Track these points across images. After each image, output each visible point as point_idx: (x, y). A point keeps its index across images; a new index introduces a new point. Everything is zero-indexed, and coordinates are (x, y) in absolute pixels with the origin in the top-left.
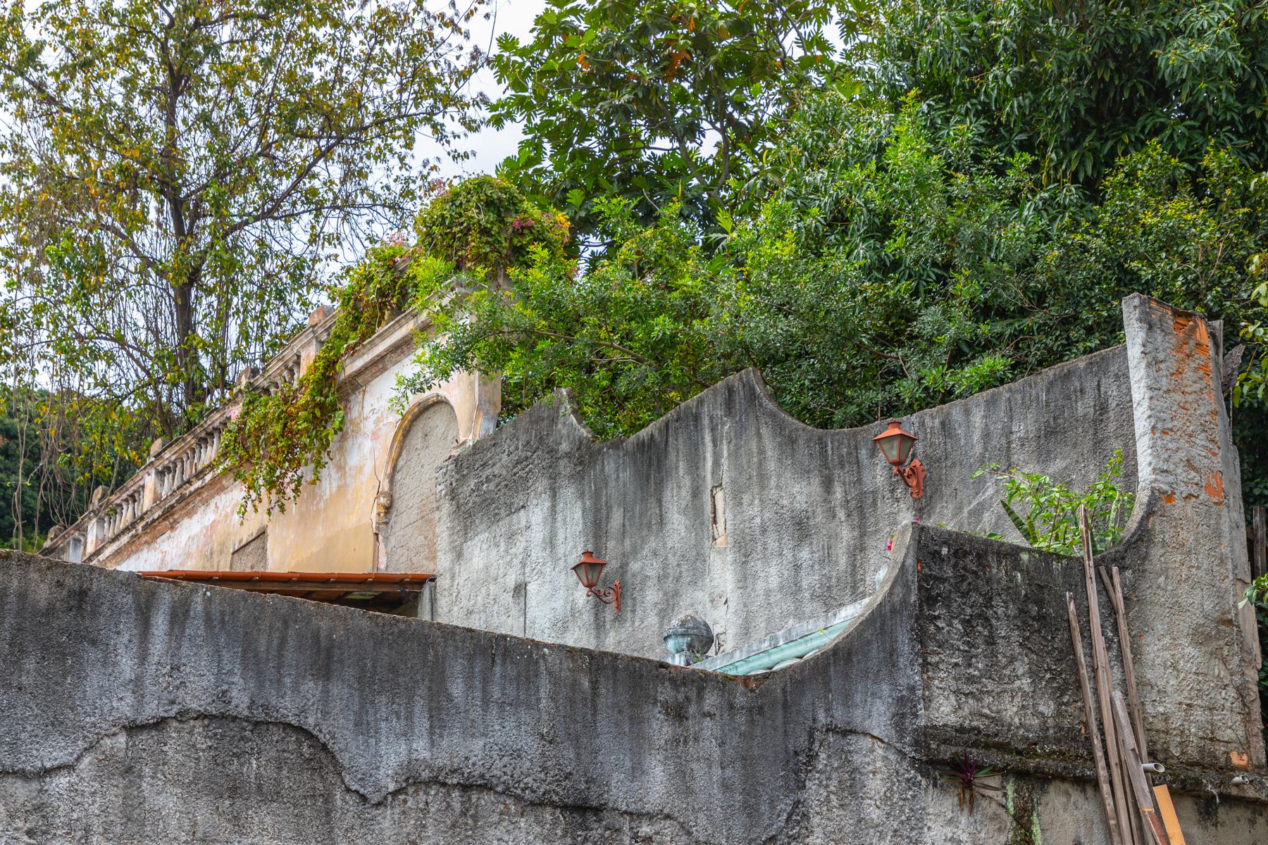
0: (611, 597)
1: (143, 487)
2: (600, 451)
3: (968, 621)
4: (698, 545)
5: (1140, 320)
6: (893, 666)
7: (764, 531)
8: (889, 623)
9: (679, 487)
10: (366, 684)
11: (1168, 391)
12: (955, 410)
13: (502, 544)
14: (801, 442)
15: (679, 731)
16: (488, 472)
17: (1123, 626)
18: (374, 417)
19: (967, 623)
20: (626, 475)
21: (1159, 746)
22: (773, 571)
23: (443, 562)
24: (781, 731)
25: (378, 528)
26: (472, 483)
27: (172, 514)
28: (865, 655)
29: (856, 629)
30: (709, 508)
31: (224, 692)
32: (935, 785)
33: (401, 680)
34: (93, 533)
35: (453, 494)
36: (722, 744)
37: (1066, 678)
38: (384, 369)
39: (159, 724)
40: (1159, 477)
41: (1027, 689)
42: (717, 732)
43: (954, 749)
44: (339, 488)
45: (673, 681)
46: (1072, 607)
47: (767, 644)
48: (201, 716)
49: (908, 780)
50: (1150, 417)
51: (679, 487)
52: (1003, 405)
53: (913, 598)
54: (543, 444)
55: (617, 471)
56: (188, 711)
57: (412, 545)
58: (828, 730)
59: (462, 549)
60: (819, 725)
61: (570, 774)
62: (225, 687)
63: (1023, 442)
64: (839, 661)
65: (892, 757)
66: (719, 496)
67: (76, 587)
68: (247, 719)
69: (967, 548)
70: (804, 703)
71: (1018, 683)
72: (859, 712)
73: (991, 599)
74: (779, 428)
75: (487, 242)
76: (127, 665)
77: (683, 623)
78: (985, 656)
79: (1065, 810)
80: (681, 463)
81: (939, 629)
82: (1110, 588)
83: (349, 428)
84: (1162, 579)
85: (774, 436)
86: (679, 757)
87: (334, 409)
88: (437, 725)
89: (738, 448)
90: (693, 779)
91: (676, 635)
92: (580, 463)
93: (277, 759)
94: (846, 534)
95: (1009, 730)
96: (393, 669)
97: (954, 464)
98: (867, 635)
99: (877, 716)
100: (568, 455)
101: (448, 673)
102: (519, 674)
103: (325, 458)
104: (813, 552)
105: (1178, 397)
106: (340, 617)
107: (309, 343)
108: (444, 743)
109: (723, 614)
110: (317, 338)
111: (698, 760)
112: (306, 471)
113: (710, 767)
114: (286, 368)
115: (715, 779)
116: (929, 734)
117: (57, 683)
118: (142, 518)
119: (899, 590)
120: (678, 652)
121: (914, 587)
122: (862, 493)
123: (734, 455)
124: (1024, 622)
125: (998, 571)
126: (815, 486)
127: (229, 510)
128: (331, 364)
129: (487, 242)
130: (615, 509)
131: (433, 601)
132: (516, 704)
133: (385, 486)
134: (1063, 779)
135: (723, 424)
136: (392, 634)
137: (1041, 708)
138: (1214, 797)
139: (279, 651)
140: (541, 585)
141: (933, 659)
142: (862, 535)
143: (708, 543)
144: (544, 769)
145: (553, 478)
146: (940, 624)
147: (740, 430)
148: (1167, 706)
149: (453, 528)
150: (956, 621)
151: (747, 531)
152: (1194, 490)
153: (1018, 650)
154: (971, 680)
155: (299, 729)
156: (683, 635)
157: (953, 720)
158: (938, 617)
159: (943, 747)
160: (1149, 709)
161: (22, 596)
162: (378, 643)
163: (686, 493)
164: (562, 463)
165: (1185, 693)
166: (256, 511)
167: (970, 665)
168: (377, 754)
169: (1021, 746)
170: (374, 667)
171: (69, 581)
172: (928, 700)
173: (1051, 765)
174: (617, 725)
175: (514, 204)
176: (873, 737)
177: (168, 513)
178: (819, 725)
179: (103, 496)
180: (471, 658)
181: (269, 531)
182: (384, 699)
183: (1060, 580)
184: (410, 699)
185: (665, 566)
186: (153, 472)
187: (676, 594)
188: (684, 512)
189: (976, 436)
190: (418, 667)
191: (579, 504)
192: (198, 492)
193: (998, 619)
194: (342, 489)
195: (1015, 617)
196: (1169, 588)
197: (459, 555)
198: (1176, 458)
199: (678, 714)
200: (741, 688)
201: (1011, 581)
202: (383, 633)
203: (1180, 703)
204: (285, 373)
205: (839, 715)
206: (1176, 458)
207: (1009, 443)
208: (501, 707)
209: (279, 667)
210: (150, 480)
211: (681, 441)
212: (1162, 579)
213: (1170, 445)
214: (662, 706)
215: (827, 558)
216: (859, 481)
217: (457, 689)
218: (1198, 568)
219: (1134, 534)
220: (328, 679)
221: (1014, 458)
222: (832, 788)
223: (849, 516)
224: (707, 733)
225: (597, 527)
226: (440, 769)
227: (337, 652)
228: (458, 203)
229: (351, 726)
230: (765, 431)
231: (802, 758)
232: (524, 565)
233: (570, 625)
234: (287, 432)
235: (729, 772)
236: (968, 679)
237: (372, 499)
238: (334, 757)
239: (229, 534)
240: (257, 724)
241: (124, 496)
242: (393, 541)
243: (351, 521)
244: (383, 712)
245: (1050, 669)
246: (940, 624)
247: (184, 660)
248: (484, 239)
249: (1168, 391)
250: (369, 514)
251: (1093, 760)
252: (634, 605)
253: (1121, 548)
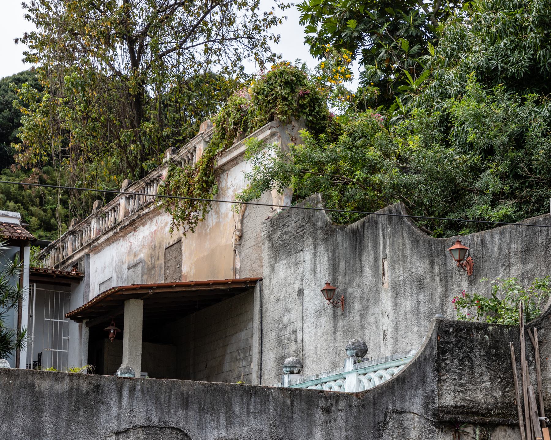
0: (340, 304)
1: (119, 204)
2: (335, 229)
4: (376, 286)
6: (424, 382)
7: (404, 283)
8: (423, 364)
9: (369, 255)
10: (201, 409)
12: (487, 234)
13: (293, 267)
14: (421, 242)
15: (328, 418)
16: (286, 229)
17: (537, 356)
18: (232, 188)
19: (460, 361)
20: (346, 244)
22: (408, 303)
23: (265, 272)
25: (236, 247)
26: (279, 233)
27: (134, 224)
28: (411, 379)
29: (407, 368)
30: (381, 268)
31: (149, 417)
32: (442, 431)
33: (215, 407)
34: (94, 225)
35: (270, 238)
36: (346, 422)
37: (508, 381)
38: (237, 164)
39: (127, 431)
41: (488, 387)
42: (344, 417)
43: (450, 416)
44: (217, 223)
45: (325, 398)
46: (512, 349)
47: (384, 360)
48: (141, 427)
49: (430, 430)
51: (369, 255)
52: (507, 235)
53: (435, 352)
55: (342, 241)
56: (136, 426)
57: (252, 258)
58: (393, 412)
59: (274, 267)
60: (389, 410)
62: (149, 416)
64: (400, 382)
65: (422, 421)
66: (386, 263)
67: (96, 384)
68: (158, 427)
70: (383, 402)
72: (407, 403)
73: (473, 349)
74: (412, 234)
75: (286, 105)
76: (114, 411)
77: (353, 344)
79: (504, 438)
80: (370, 244)
81: (447, 364)
82: (532, 338)
87: (213, 182)
90: (333, 436)
91: (350, 349)
92: (327, 234)
94: (440, 289)
95: (479, 405)
96: (212, 403)
97: (486, 261)
98: (413, 370)
99: (416, 404)
100: (321, 228)
101: (233, 403)
102: (261, 401)
103: (208, 208)
104: (425, 296)
107: (200, 141)
108: (232, 430)
109: (386, 321)
110: (204, 140)
111: (336, 429)
113: (341, 431)
114: (189, 152)
115: (343, 436)
116: (442, 409)
117: (91, 419)
118: (119, 224)
119: (428, 350)
120: (352, 356)
121: (436, 348)
122: (447, 270)
123: (392, 244)
124: (489, 358)
125: (477, 336)
126: (427, 264)
127: (163, 225)
128: (211, 160)
129: (286, 105)
130: (342, 260)
131: (261, 291)
132: (260, 413)
133: (239, 226)
134: (504, 425)
135: (387, 228)
139: (169, 400)
140: (310, 291)
141: (443, 378)
142: (446, 290)
143: (381, 286)
145: (315, 238)
146: (447, 362)
147: (395, 233)
149: (270, 255)
150: (455, 360)
151: (397, 282)
153: (484, 370)
154: (461, 385)
155: (177, 429)
156: (353, 349)
157: (452, 403)
158: (447, 359)
161: (78, 389)
162: (206, 394)
163: (371, 258)
164: (319, 232)
166: (178, 230)
167: (461, 379)
169: (484, 412)
170: (204, 403)
171: (93, 382)
172: (440, 396)
174: (301, 417)
175: (300, 81)
176: (414, 413)
177: (132, 223)
178: (389, 410)
179: (99, 207)
180: (242, 396)
181: (183, 240)
182: (208, 415)
183: (507, 337)
184: (219, 414)
185: (363, 293)
186: (124, 198)
187: (367, 307)
188: (371, 268)
189: (496, 248)
191: (326, 254)
192: (147, 214)
193: (476, 357)
194: (218, 224)
195: (484, 356)
197: (273, 270)
199: (327, 411)
200: (355, 398)
204: (189, 155)
205: (399, 406)
207: (510, 253)
208: (254, 414)
209: (169, 407)
210: (122, 202)
211: (370, 233)
214: (321, 408)
215: (431, 300)
216: (445, 264)
217: (237, 409)
219: (546, 312)
221: (512, 260)
222: (395, 436)
223: (441, 280)
224: (340, 417)
228: (270, 83)
229: (196, 426)
231: (381, 425)
232: (302, 280)
234: (189, 192)
235: (349, 433)
236: (460, 385)
237: (232, 232)
239: (163, 239)
241: (110, 208)
242: (243, 254)
245: (500, 377)
246: (447, 362)
247: (134, 407)
248: (284, 103)
250: (231, 239)
251: (518, 416)
253: (539, 319)
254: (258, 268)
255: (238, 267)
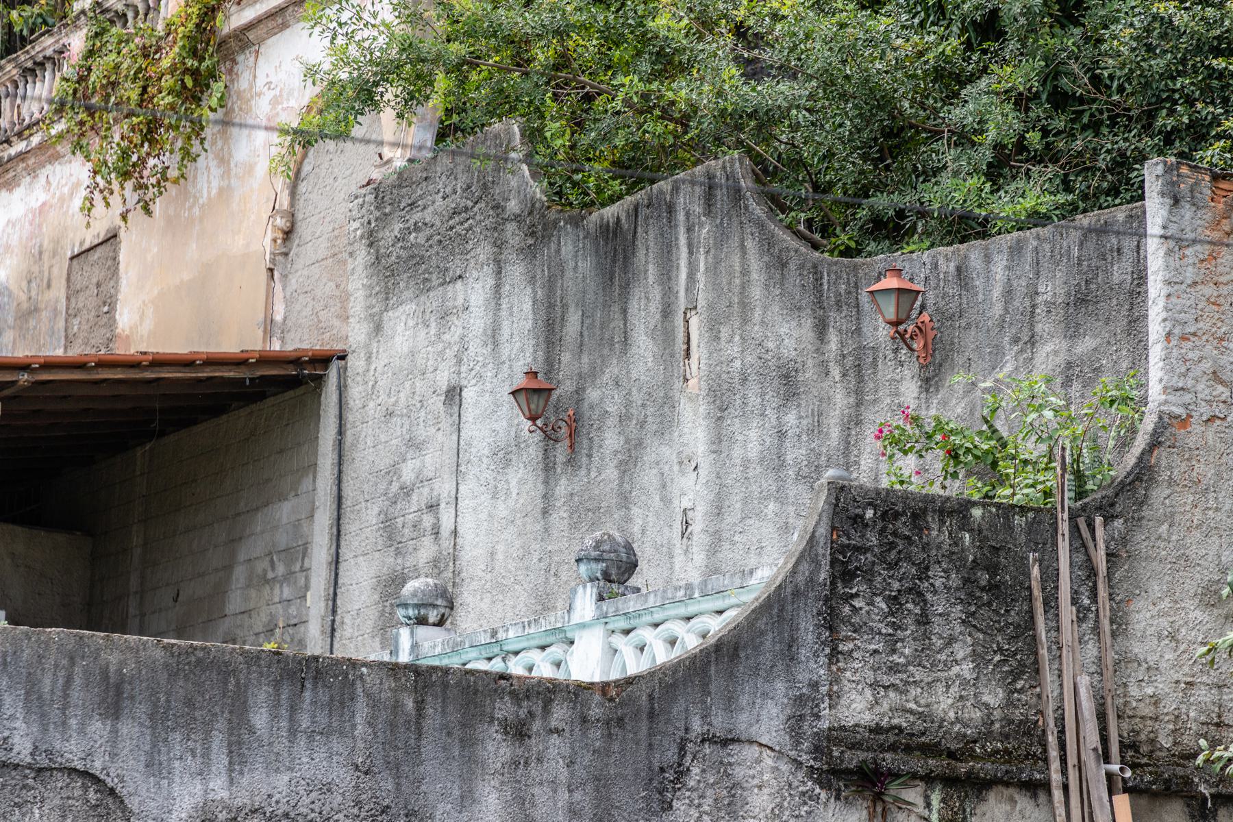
0: (564, 431)
3: (895, 598)
4: (666, 384)
5: (1163, 194)
6: (792, 659)
7: (744, 380)
8: (789, 608)
10: (158, 720)
11: (1195, 283)
12: (973, 251)
13: (433, 325)
14: (792, 266)
15: (519, 751)
16: (417, 216)
17: (1103, 593)
18: (269, 95)
19: (893, 600)
20: (586, 265)
21: (1143, 737)
22: (753, 434)
23: (355, 334)
24: (644, 745)
25: (273, 261)
26: (397, 227)
29: (746, 618)
30: (681, 337)
31: (5, 739)
32: (838, 798)
33: (198, 714)
35: (371, 238)
37: (1021, 661)
38: (285, 26)
40: (1171, 398)
41: (968, 676)
42: (566, 750)
43: (862, 755)
44: (221, 190)
45: (514, 695)
46: (1035, 572)
49: (803, 794)
50: (1165, 320)
52: (1029, 256)
53: (823, 576)
54: (484, 190)
55: (574, 255)
57: (319, 293)
58: (703, 741)
59: (381, 320)
60: (692, 735)
61: (388, 807)
62: (6, 734)
63: (1050, 305)
64: (723, 660)
66: (694, 321)
68: (29, 766)
69: (899, 508)
70: (675, 711)
71: (956, 669)
73: (927, 568)
74: (768, 243)
77: (598, 544)
78: (915, 639)
80: (651, 266)
81: (855, 610)
82: (1090, 544)
83: (234, 103)
84: (1165, 526)
85: (762, 252)
86: (519, 782)
87: (213, 75)
88: (238, 757)
89: (717, 262)
90: (534, 805)
92: (533, 234)
93: (62, 807)
94: (841, 400)
95: (940, 727)
96: (189, 702)
98: (761, 624)
99: (766, 719)
100: (517, 218)
101: (250, 702)
102: (332, 699)
103: (196, 147)
104: (800, 417)
105: (1209, 290)
106: (132, 648)
108: (245, 781)
109: (692, 483)
111: (541, 784)
112: (171, 160)
113: (555, 791)
115: (560, 804)
116: (840, 736)
119: (805, 567)
120: (591, 580)
121: (825, 563)
122: (861, 348)
123: (713, 270)
124: (970, 594)
125: (938, 534)
126: (806, 329)
127: (66, 190)
130: (572, 309)
131: (342, 389)
132: (326, 733)
134: (1007, 784)
135: (701, 225)
136: (189, 663)
137: (986, 698)
138: (1205, 800)
142: (859, 404)
143: (678, 384)
144: (358, 803)
145: (499, 245)
146: (857, 603)
147: (721, 237)
148: (1162, 685)
149: (371, 287)
150: (878, 599)
151: (724, 376)
152: (1219, 410)
153: (958, 629)
154: (894, 669)
155: (85, 774)
156: (597, 560)
157: (867, 718)
159: (848, 755)
160: (1134, 691)
162: (173, 675)
163: (655, 307)
164: (511, 227)
165: (1186, 669)
166: (108, 205)
167: (894, 651)
168: (170, 797)
169: (954, 746)
170: (168, 701)
173: (988, 768)
174: (445, 749)
176: (761, 745)
178: (692, 735)
180: (277, 685)
181: (122, 234)
182: (178, 736)
185: (628, 404)
187: (640, 444)
188: (652, 334)
189: (997, 292)
190: (217, 698)
191: (529, 291)
192: (22, 156)
193: (935, 592)
194: (225, 193)
195: (958, 589)
196: (1174, 538)
197: (378, 328)
198: (1197, 371)
199: (519, 732)
200: (597, 697)
201: (956, 544)
202: (178, 663)
203: (1177, 682)
205: (719, 723)
206: (1197, 371)
208: (311, 736)
209: (64, 709)
212: (1165, 526)
213: (1191, 355)
215: (816, 429)
216: (858, 330)
217: (260, 719)
218: (1217, 509)
219: (1129, 474)
220: (117, 718)
221: (1039, 328)
222: (706, 808)
223: (844, 375)
224: (553, 752)
225: (550, 330)
226: (240, 810)
227: (127, 687)
229: (141, 768)
230: (750, 244)
231: (670, 775)
232: (459, 362)
233: (514, 458)
235: (578, 796)
236: (891, 668)
238: (122, 802)
240: (40, 770)
242: (293, 282)
243: (236, 244)
244: (177, 750)
245: (1000, 650)
246: (857, 603)
249: (1195, 283)
250: (264, 242)
251: (1046, 760)
252: (591, 448)
253: (1110, 492)
254: (336, 323)
255: (278, 318)
